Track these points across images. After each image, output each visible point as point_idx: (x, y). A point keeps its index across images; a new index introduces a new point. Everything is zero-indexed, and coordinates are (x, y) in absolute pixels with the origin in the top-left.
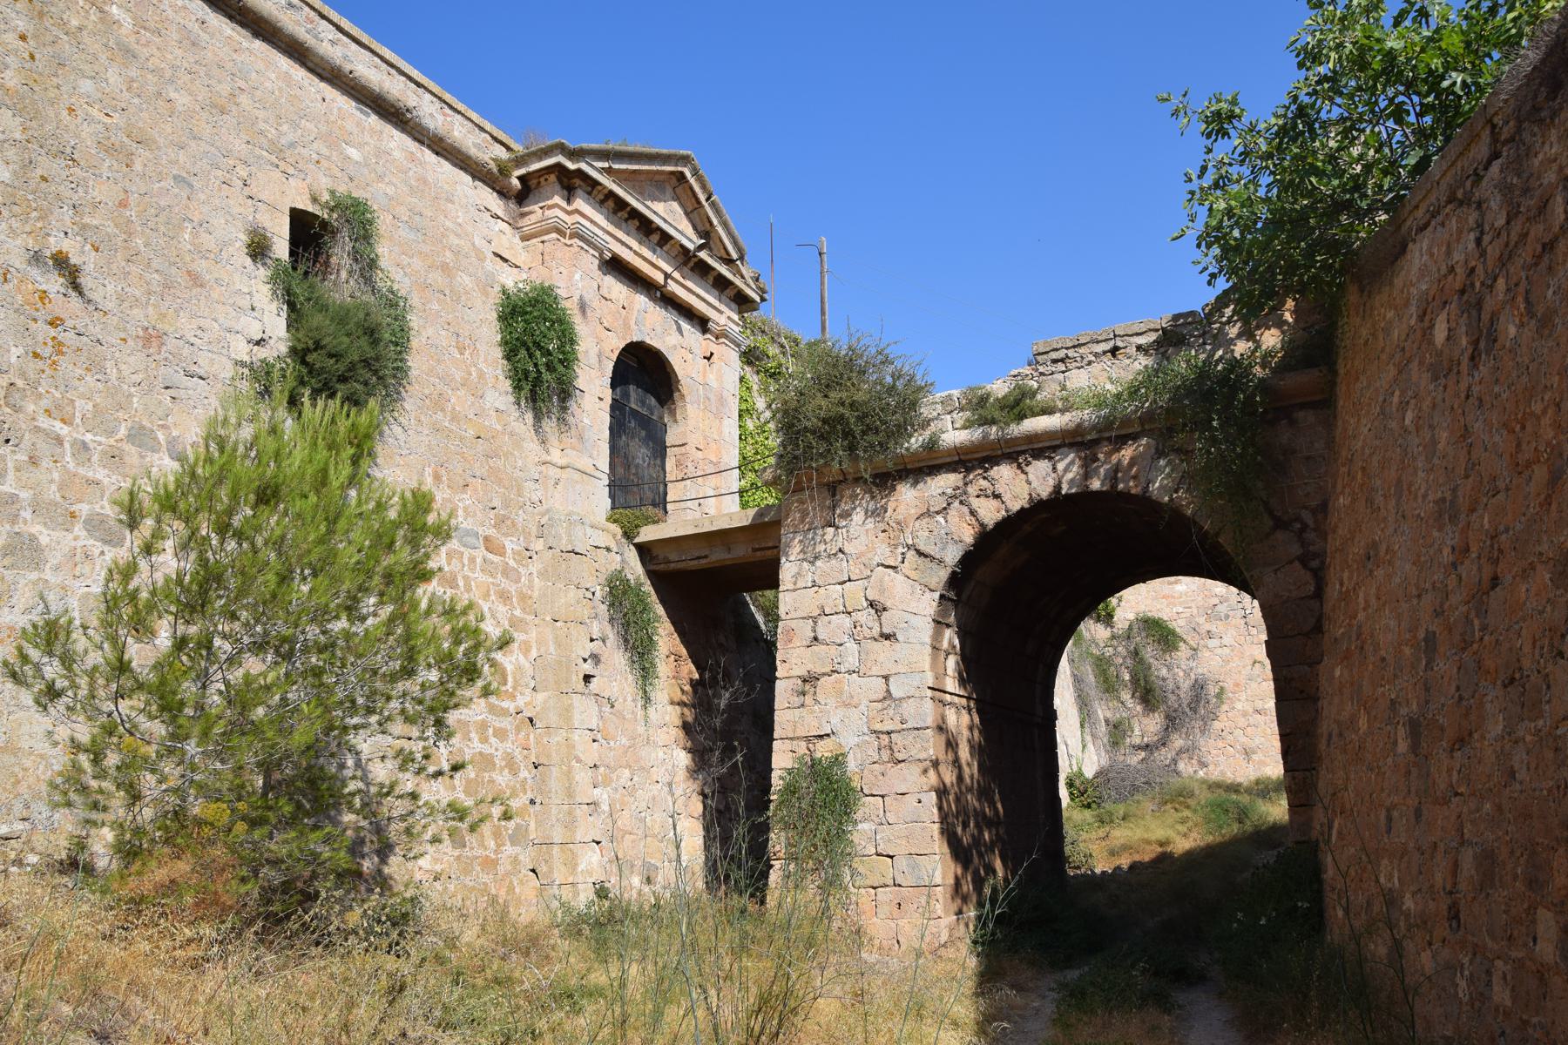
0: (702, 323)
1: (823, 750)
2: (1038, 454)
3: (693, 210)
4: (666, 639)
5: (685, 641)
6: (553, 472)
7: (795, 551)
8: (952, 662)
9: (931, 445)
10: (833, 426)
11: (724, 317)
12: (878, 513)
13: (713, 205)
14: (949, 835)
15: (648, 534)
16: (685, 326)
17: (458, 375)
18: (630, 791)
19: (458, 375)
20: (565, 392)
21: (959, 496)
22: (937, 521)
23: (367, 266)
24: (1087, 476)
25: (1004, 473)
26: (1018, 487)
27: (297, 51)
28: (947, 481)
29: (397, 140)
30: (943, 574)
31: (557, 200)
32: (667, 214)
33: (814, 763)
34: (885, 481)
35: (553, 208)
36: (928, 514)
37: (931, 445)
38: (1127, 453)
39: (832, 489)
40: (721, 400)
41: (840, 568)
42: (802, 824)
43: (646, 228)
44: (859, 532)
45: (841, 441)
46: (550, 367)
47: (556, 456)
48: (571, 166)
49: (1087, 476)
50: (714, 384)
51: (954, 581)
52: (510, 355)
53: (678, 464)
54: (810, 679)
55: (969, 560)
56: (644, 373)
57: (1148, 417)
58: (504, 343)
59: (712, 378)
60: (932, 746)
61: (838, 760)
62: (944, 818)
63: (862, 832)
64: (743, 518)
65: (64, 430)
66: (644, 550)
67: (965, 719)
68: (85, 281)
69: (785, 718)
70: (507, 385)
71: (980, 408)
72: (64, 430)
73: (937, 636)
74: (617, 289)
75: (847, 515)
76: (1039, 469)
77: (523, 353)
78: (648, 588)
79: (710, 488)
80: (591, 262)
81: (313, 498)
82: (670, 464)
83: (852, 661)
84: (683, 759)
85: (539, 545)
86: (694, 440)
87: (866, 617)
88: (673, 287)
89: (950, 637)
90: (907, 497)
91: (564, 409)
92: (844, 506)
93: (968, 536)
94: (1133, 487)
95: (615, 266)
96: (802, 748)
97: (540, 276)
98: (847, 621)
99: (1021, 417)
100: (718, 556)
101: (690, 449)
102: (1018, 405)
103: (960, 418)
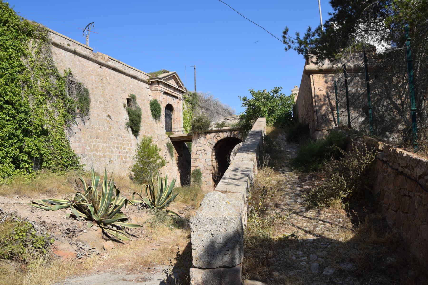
0: (177, 98)
1: (198, 168)
2: (225, 132)
3: (176, 80)
4: (174, 151)
5: (177, 151)
6: (158, 128)
7: (194, 142)
8: (214, 157)
9: (212, 129)
10: (199, 128)
11: (180, 96)
12: (205, 138)
13: (179, 79)
14: (213, 179)
15: (172, 136)
16: (174, 99)
17: (146, 116)
18: (171, 173)
19: (146, 116)
20: (160, 116)
21: (215, 136)
22: (212, 139)
23: (135, 103)
24: (231, 135)
25: (221, 134)
26: (223, 136)
27: (124, 73)
28: (213, 134)
29: (136, 81)
30: (213, 146)
31: (157, 85)
32: (172, 82)
33: (196, 170)
34: (205, 133)
35: (156, 87)
36: (211, 138)
37: (212, 129)
38: (236, 132)
39: (199, 134)
40: (180, 110)
41: (200, 144)
42: (195, 178)
43: (169, 86)
44: (202, 140)
45: (200, 129)
46: (158, 113)
47: (158, 126)
48: (159, 80)
49: (231, 135)
50: (179, 107)
51: (214, 147)
52: (152, 111)
53: (174, 121)
54: (196, 159)
55: (216, 144)
56: (169, 108)
57: (238, 128)
58: (151, 109)
59: (178, 107)
60: (211, 168)
61: (199, 169)
62: (213, 177)
63: (203, 179)
64: (185, 134)
65: (112, 137)
66: (171, 138)
67: (216, 164)
68: (111, 118)
69: (193, 164)
70: (152, 116)
71: (218, 125)
72: (112, 137)
73: (212, 154)
74: (165, 96)
75: (201, 138)
76: (225, 133)
77: (154, 111)
78: (172, 144)
79: (179, 130)
80: (162, 93)
81: (32, 72)
82: (172, 121)
83: (201, 157)
84: (177, 168)
85: (158, 139)
86: (176, 117)
87: (203, 151)
88: (173, 94)
89: (214, 154)
90: (208, 136)
91: (159, 118)
92: (200, 136)
93: (216, 142)
94: (236, 137)
95: (166, 93)
96: (195, 168)
97: (155, 98)
98: (201, 152)
99: (223, 127)
100: (182, 139)
101: (175, 119)
102: (223, 125)
103: (215, 126)
